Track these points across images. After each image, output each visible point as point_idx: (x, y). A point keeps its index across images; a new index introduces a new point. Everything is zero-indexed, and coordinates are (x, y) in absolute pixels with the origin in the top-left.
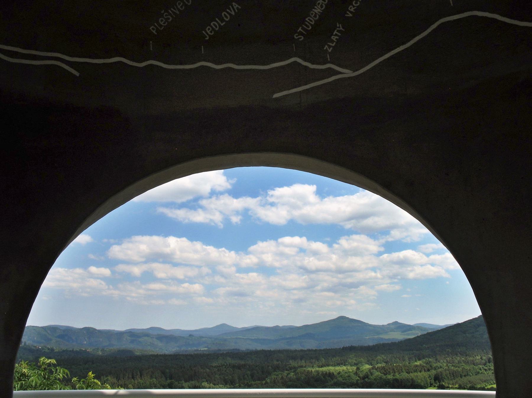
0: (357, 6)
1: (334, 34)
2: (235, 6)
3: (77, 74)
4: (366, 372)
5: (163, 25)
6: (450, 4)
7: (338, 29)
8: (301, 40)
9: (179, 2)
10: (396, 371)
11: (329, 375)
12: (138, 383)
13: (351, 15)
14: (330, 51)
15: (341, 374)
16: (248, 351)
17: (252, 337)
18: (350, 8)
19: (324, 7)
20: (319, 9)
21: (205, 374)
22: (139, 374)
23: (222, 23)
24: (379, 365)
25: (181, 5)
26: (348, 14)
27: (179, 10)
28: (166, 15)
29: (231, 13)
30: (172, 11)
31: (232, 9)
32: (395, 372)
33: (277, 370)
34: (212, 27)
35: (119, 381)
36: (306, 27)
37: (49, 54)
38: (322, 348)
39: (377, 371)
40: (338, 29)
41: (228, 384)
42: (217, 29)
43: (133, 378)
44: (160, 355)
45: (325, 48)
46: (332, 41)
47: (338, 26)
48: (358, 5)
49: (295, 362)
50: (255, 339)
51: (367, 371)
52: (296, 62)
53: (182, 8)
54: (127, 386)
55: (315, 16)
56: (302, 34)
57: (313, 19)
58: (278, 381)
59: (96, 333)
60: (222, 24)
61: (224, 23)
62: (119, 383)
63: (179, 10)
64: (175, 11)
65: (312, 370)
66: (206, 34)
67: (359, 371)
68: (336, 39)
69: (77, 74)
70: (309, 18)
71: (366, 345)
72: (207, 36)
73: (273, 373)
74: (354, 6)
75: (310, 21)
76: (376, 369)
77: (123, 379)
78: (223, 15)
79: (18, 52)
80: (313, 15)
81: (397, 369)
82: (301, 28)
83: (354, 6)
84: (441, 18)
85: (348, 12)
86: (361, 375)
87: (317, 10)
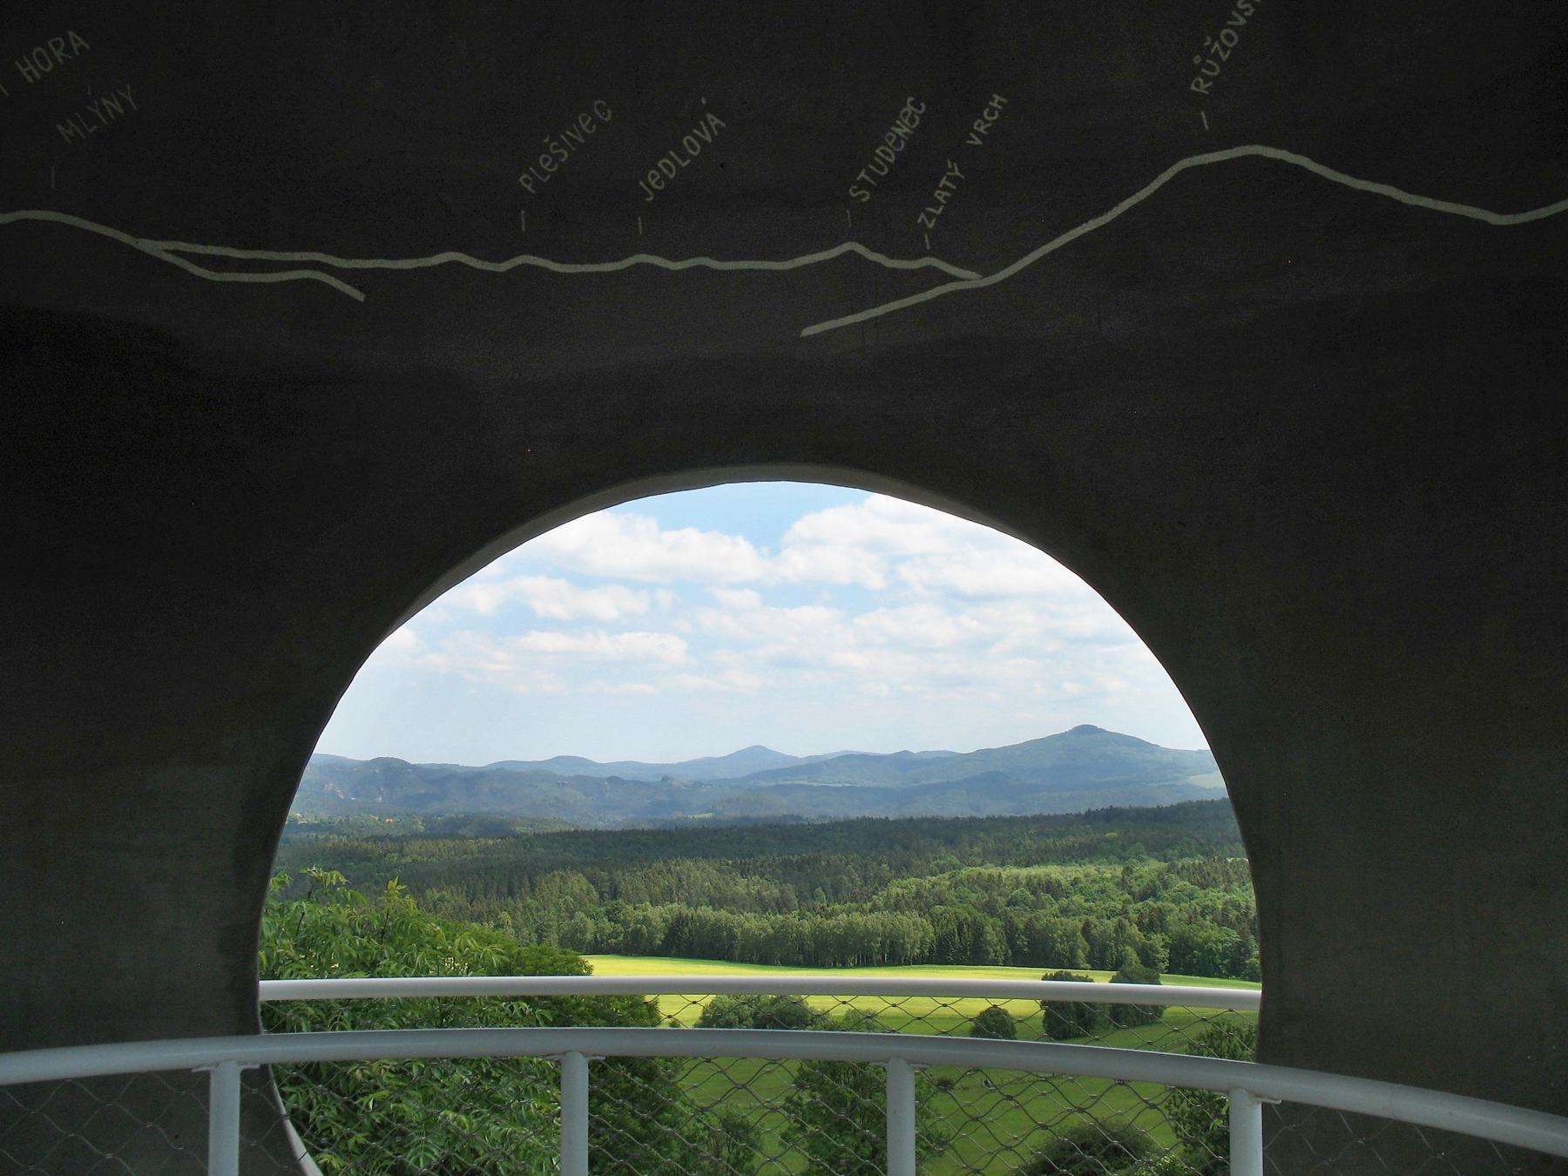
0: (993, 121)
1: (941, 185)
2: (713, 120)
3: (359, 296)
4: (1151, 881)
5: (549, 170)
6: (1202, 125)
7: (949, 174)
8: (864, 200)
9: (584, 115)
10: (1234, 877)
11: (1048, 887)
12: (524, 908)
13: (978, 142)
14: (931, 226)
15: (1080, 885)
16: (826, 822)
17: (834, 783)
18: (976, 124)
19: (917, 122)
20: (904, 127)
21: (707, 884)
22: (527, 883)
23: (683, 162)
24: (1187, 861)
25: (588, 122)
26: (972, 139)
27: (584, 134)
28: (555, 147)
29: (703, 137)
30: (567, 136)
31: (704, 128)
32: (1230, 882)
33: (904, 874)
34: (659, 170)
35: (474, 903)
36: (878, 168)
37: (298, 256)
38: (1029, 814)
39: (1182, 879)
40: (949, 174)
41: (770, 910)
42: (672, 176)
43: (511, 893)
44: (584, 833)
45: (919, 221)
46: (937, 204)
47: (950, 166)
48: (995, 118)
49: (954, 851)
50: (843, 787)
51: (1154, 876)
52: (852, 252)
53: (591, 129)
54: (497, 917)
55: (897, 143)
56: (868, 187)
57: (892, 149)
58: (906, 901)
59: (408, 773)
60: (684, 165)
61: (688, 162)
62: (475, 907)
63: (584, 134)
64: (575, 137)
65: (1000, 874)
66: (647, 189)
67: (1132, 878)
68: (945, 198)
69: (359, 296)
70: (882, 148)
71: (1152, 805)
72: (650, 193)
73: (895, 881)
74: (986, 122)
75: (887, 154)
76: (1178, 872)
77: (485, 896)
78: (685, 143)
79: (229, 257)
80: (893, 141)
81: (1236, 873)
82: (864, 171)
83: (986, 122)
84: (1181, 158)
85: (972, 135)
86: (1136, 889)
87: (902, 128)
